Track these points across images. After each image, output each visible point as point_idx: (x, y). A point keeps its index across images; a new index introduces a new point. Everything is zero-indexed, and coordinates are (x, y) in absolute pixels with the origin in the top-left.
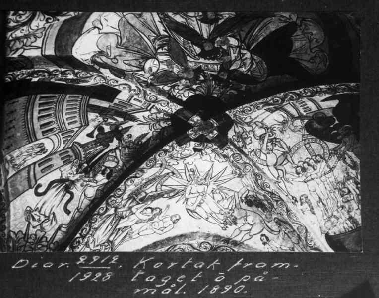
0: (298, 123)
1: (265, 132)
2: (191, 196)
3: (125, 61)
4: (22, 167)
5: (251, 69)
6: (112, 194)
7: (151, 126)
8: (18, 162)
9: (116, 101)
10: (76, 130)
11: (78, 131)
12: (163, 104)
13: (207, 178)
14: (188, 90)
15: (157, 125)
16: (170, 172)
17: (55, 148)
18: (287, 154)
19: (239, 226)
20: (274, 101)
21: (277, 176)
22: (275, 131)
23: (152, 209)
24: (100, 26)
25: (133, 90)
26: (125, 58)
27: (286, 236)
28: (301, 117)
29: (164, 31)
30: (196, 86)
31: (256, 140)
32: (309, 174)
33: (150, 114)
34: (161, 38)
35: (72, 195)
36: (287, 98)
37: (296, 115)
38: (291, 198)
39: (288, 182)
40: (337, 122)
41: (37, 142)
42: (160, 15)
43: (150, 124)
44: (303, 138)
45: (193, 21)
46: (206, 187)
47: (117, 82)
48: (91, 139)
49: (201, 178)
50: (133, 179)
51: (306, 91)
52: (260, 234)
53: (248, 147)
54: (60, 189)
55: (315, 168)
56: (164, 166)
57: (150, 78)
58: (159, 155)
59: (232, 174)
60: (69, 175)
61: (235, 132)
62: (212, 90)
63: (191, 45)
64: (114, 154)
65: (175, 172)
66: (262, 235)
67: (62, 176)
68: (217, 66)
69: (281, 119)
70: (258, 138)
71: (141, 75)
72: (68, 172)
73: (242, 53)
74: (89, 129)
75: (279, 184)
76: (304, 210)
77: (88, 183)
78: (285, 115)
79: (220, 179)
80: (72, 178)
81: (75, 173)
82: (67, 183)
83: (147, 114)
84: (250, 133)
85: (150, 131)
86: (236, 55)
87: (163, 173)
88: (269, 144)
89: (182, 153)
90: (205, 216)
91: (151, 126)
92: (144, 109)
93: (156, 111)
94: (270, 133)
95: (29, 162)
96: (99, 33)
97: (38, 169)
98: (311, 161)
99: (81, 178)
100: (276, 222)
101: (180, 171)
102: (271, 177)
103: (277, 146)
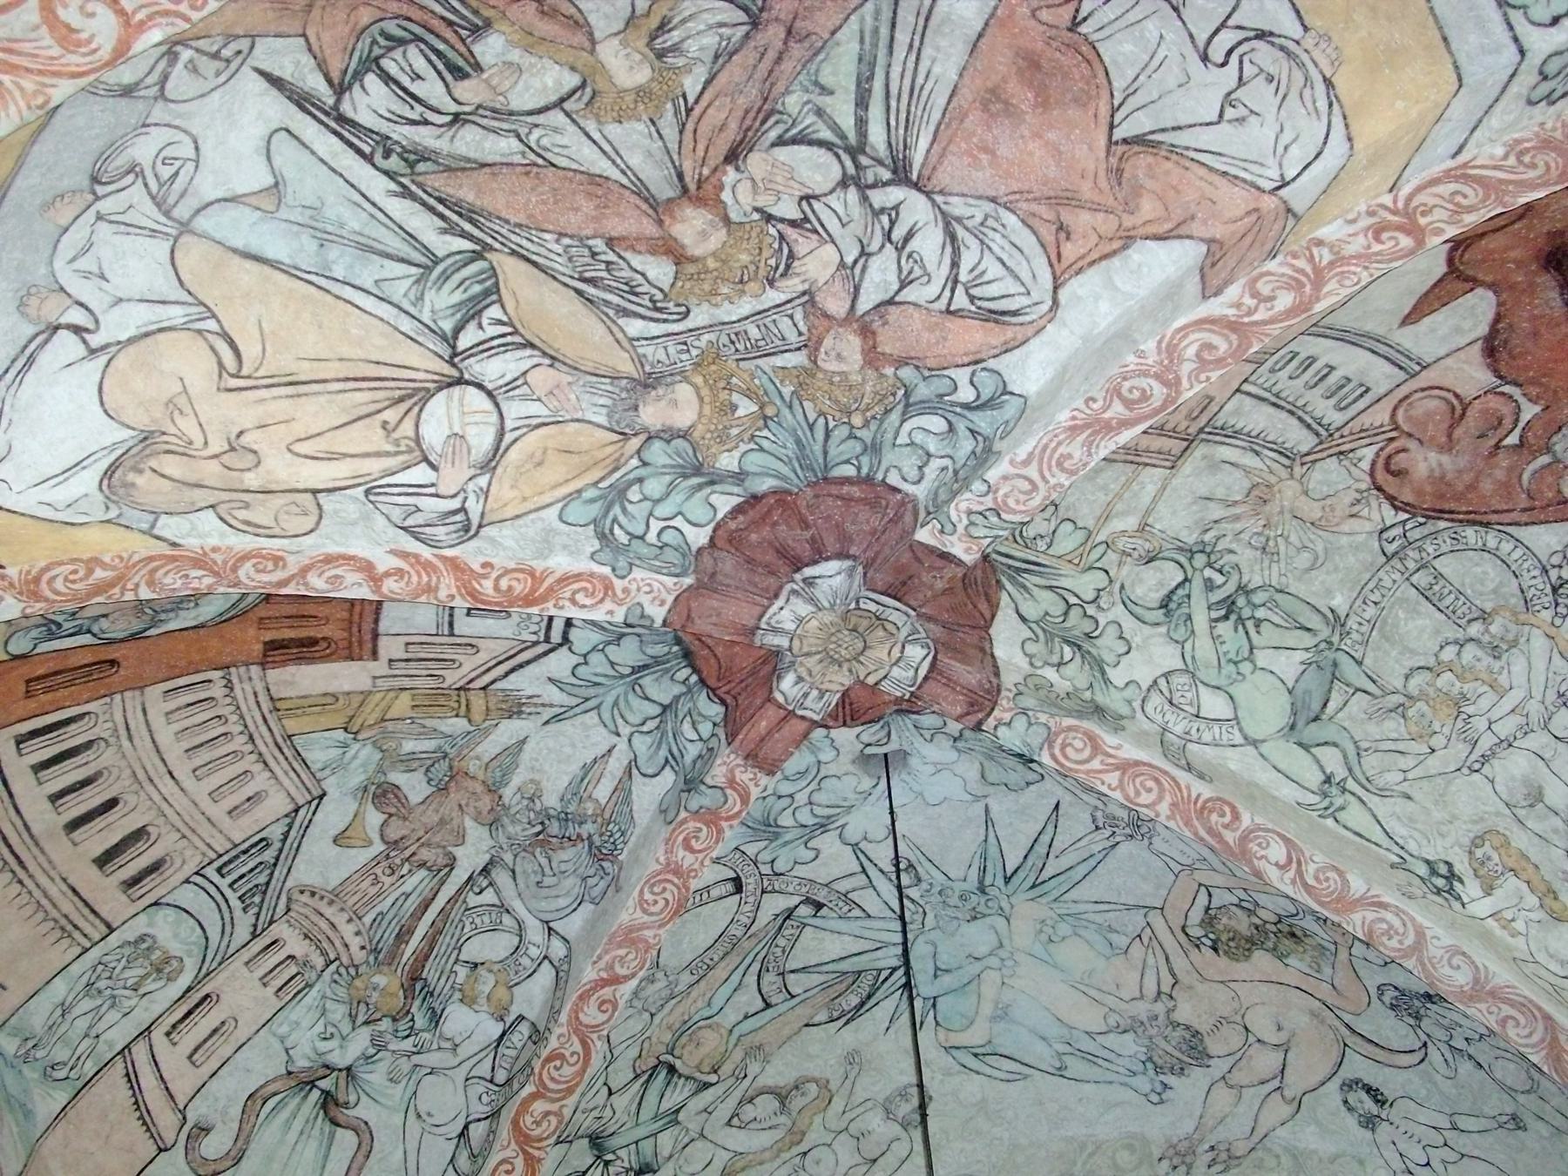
0: (1329, 474)
1: (1180, 578)
2: (946, 981)
3: (298, 448)
4: (89, 1068)
5: (963, 277)
6: (529, 1089)
7: (606, 716)
8: (61, 1054)
9: (390, 648)
10: (276, 832)
11: (286, 835)
12: (580, 597)
13: (988, 881)
14: (700, 487)
15: (636, 702)
16: (796, 900)
17: (214, 935)
18: (1333, 647)
19: (1219, 1067)
20: (1128, 404)
21: (1314, 778)
22: (1228, 558)
23: (782, 1096)
24: (76, 316)
25: (387, 574)
26: (299, 429)
27: (1466, 1067)
28: (1330, 443)
29: (444, 232)
30: (737, 454)
31: (1147, 630)
32: (1480, 724)
33: (575, 660)
34: (445, 277)
35: (363, 1131)
36: (1181, 361)
37: (1300, 439)
38: (1423, 870)
39: (1383, 793)
40: (1529, 411)
41: (114, 939)
42: (378, 159)
43: (598, 707)
44: (1390, 549)
45: (556, 130)
46: (1000, 922)
47: (278, 560)
48: (360, 857)
49: (959, 887)
50: (607, 992)
51: (1264, 288)
52: (1337, 1081)
53: (1117, 676)
54: (298, 1125)
55: (1503, 680)
56: (750, 883)
57: (471, 486)
58: (687, 846)
59: (1097, 828)
60: (323, 1046)
61: (1023, 619)
62: (818, 448)
63: (611, 257)
64: (489, 896)
65: (821, 896)
66: (1350, 1085)
67: (290, 1059)
68: (791, 317)
69: (1236, 484)
70: (1159, 615)
71: (417, 489)
72: (308, 1032)
73: (882, 210)
74: (333, 816)
75: (1341, 816)
76: (1508, 915)
77: (416, 1059)
78: (1250, 460)
79: (1046, 874)
80: (340, 1059)
81: (346, 1027)
82: (323, 1084)
83: (560, 663)
84: (1103, 603)
85: (615, 739)
86: (856, 228)
87: (764, 917)
88: (1224, 629)
89: (816, 797)
90: (1042, 1054)
91: (606, 716)
92: (535, 643)
93: (596, 637)
94: (1208, 573)
95: (118, 1036)
96: (93, 352)
97: (172, 1058)
98: (1470, 652)
99: (379, 1045)
100: (1393, 1007)
101: (842, 886)
102: (1288, 792)
103: (1265, 626)
